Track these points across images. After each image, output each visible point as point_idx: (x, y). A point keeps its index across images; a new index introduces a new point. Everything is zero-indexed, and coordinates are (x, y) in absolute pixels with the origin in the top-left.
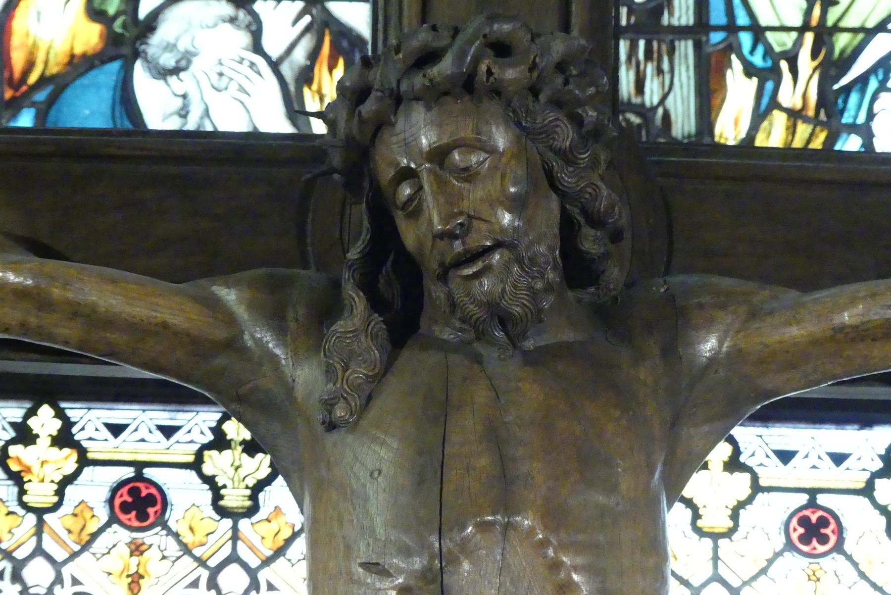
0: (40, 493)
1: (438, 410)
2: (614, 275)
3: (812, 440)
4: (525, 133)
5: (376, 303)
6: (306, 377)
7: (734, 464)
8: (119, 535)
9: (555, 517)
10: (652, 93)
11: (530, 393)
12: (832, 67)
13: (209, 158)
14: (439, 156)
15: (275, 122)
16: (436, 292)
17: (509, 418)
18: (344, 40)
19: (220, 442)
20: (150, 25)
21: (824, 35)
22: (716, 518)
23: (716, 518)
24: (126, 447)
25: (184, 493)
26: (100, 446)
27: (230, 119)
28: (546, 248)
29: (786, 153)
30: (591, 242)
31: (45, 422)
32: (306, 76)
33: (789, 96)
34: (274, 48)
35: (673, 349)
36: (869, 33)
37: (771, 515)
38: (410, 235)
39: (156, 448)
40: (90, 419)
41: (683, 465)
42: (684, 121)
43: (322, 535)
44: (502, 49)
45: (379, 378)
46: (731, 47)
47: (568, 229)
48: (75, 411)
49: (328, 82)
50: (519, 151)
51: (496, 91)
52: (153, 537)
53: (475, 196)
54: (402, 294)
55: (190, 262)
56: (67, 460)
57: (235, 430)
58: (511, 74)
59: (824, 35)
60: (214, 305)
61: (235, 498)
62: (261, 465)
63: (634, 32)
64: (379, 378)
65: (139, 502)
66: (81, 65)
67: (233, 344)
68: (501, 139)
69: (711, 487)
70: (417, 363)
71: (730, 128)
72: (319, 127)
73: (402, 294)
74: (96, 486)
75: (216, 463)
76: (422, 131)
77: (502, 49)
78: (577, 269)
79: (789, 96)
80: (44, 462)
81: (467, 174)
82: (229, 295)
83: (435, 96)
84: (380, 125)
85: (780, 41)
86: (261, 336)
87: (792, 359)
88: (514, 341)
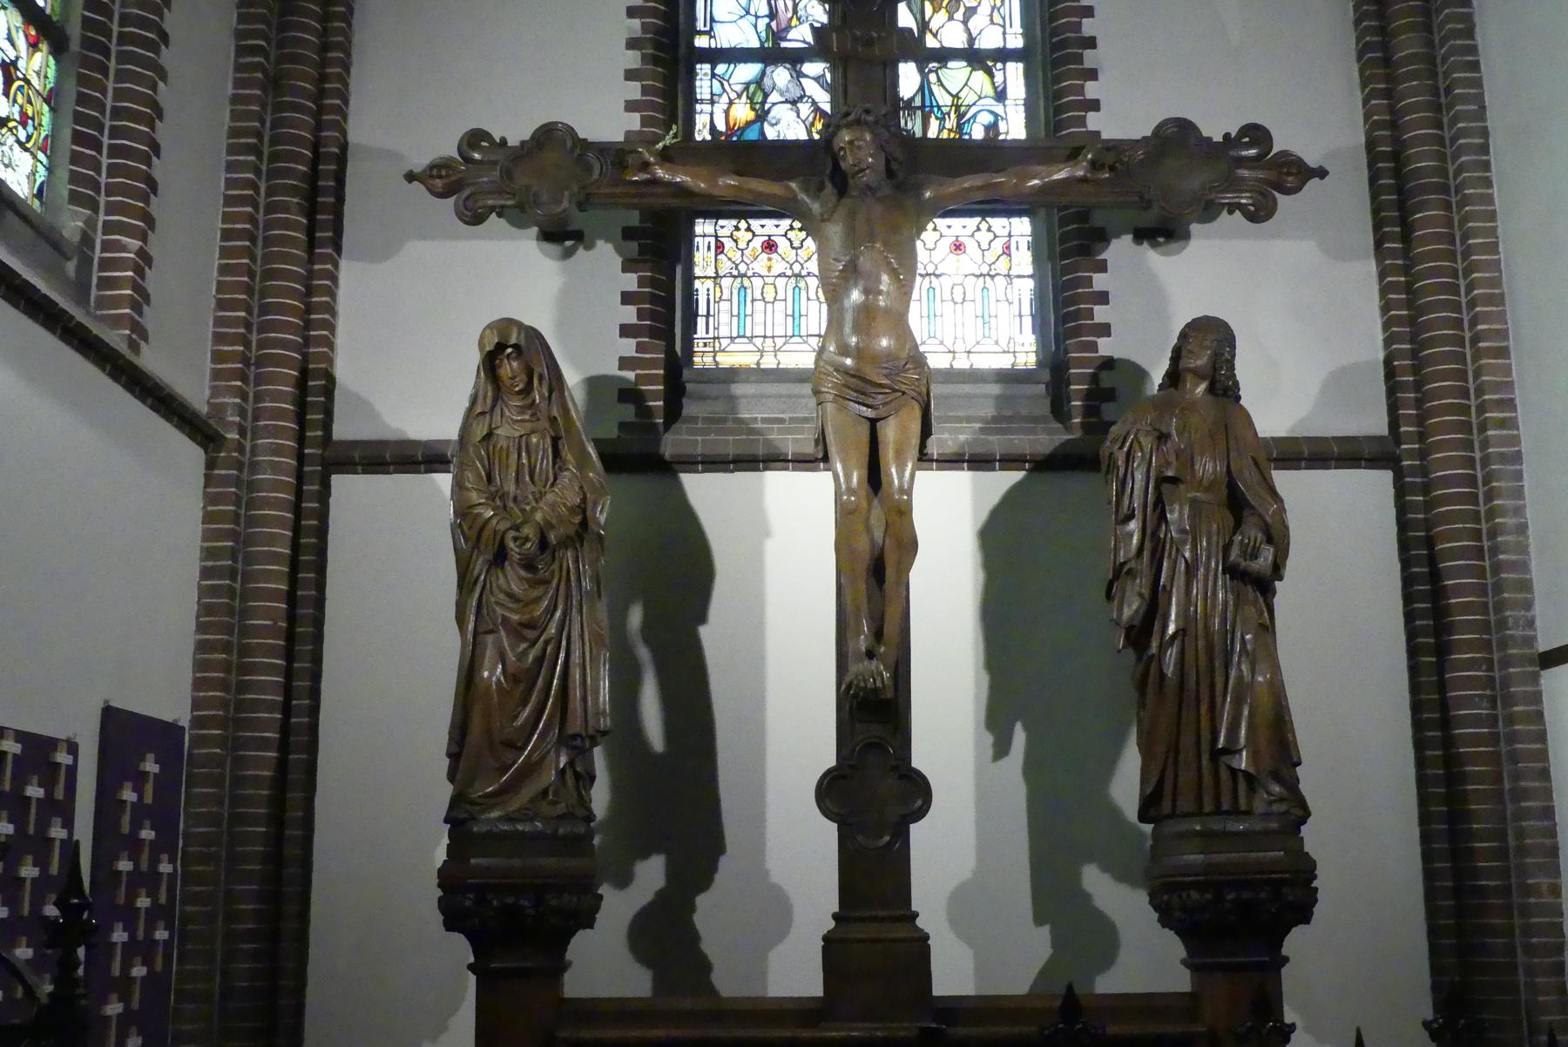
0: (742, 245)
1: (852, 215)
2: (901, 175)
3: (770, 223)
4: (875, 135)
5: (835, 185)
6: (816, 207)
7: (935, 229)
8: (765, 256)
9: (886, 244)
10: (910, 126)
11: (878, 210)
12: (960, 116)
13: (783, 146)
14: (851, 142)
15: (803, 136)
16: (851, 182)
17: (80, 224)
18: (823, 113)
19: (792, 228)
20: (769, 111)
21: (958, 107)
22: (930, 245)
23: (930, 245)
24: (766, 231)
25: (783, 244)
26: (758, 231)
27: (791, 137)
28: (882, 167)
29: (948, 139)
30: (894, 166)
31: (743, 225)
32: (812, 124)
33: (948, 125)
34: (803, 116)
35: (919, 195)
36: (969, 106)
37: (946, 244)
38: (843, 165)
39: (774, 231)
40: (755, 224)
41: (924, 229)
42: (919, 134)
43: (821, 251)
44: (867, 112)
45: (836, 207)
46: (932, 112)
47: (888, 163)
48: (751, 221)
49: (819, 126)
50: (873, 140)
51: (866, 123)
52: (774, 256)
53: (861, 154)
54: (841, 182)
55: (781, 176)
56: (749, 235)
57: (797, 224)
58: (870, 119)
59: (958, 107)
60: (790, 188)
61: (796, 244)
62: (803, 234)
63: (904, 109)
64: (836, 207)
65: (770, 246)
66: (749, 124)
67: (794, 199)
68: (868, 137)
69: (928, 236)
70: (847, 201)
71: (932, 134)
72: (817, 137)
73: (841, 182)
74: (758, 243)
75: (791, 234)
76: (846, 136)
77: (867, 112)
78: (890, 173)
79: (948, 125)
80: (744, 236)
81: (859, 148)
82: (793, 185)
83: (849, 126)
84: (834, 134)
85: (945, 110)
86: (802, 196)
87: (952, 197)
88: (873, 194)
